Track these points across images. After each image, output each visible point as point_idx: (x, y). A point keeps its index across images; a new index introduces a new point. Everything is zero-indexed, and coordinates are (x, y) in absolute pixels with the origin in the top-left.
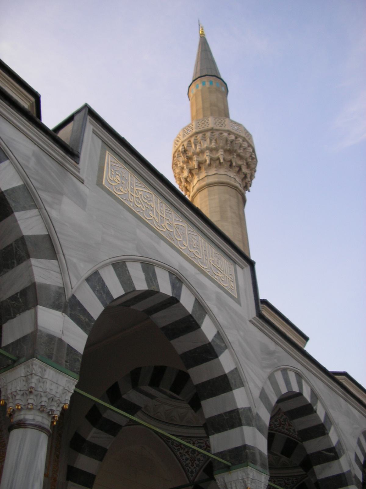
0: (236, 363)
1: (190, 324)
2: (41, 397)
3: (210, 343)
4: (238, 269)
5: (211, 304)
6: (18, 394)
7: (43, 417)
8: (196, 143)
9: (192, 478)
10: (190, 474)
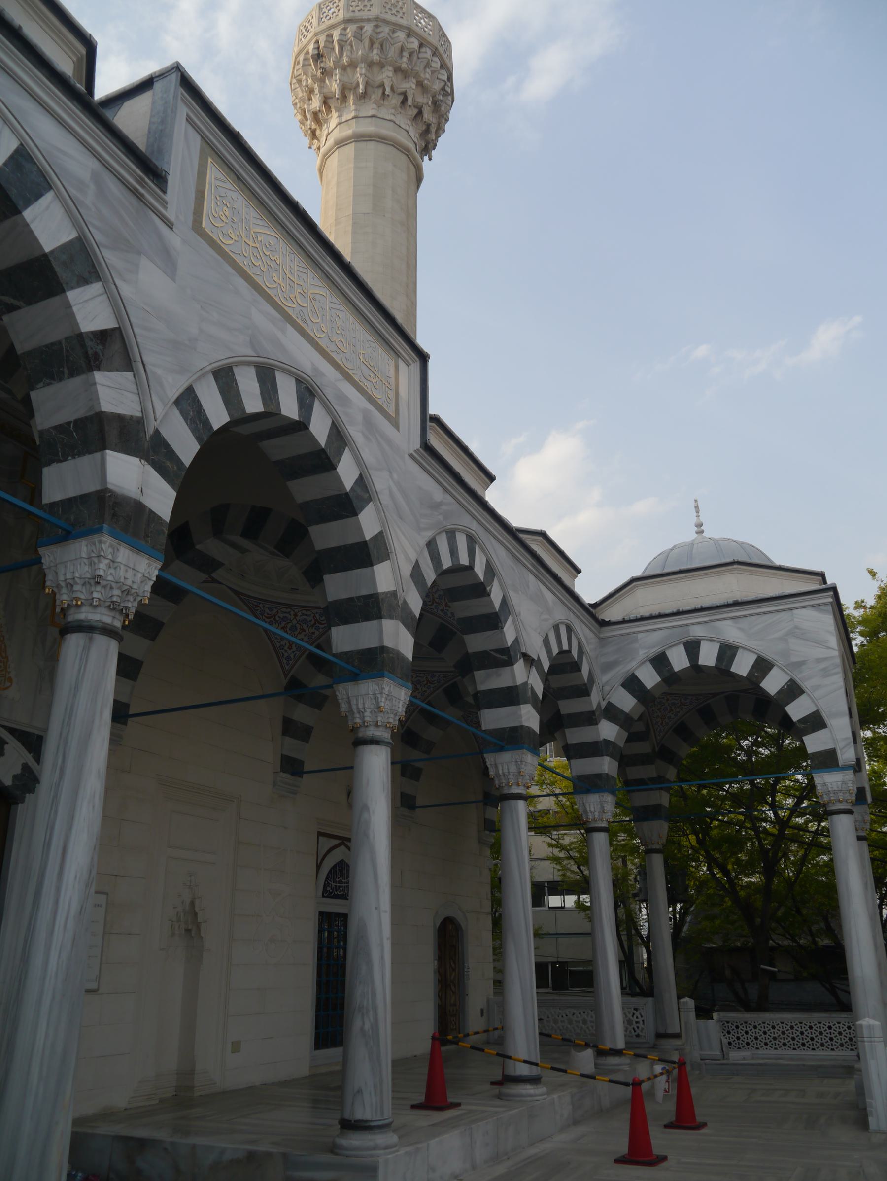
0: (383, 525)
1: (322, 462)
2: (112, 588)
3: (347, 494)
4: (402, 365)
5: (355, 432)
6: (77, 584)
7: (114, 618)
8: (343, 43)
9: (287, 667)
10: (285, 661)
